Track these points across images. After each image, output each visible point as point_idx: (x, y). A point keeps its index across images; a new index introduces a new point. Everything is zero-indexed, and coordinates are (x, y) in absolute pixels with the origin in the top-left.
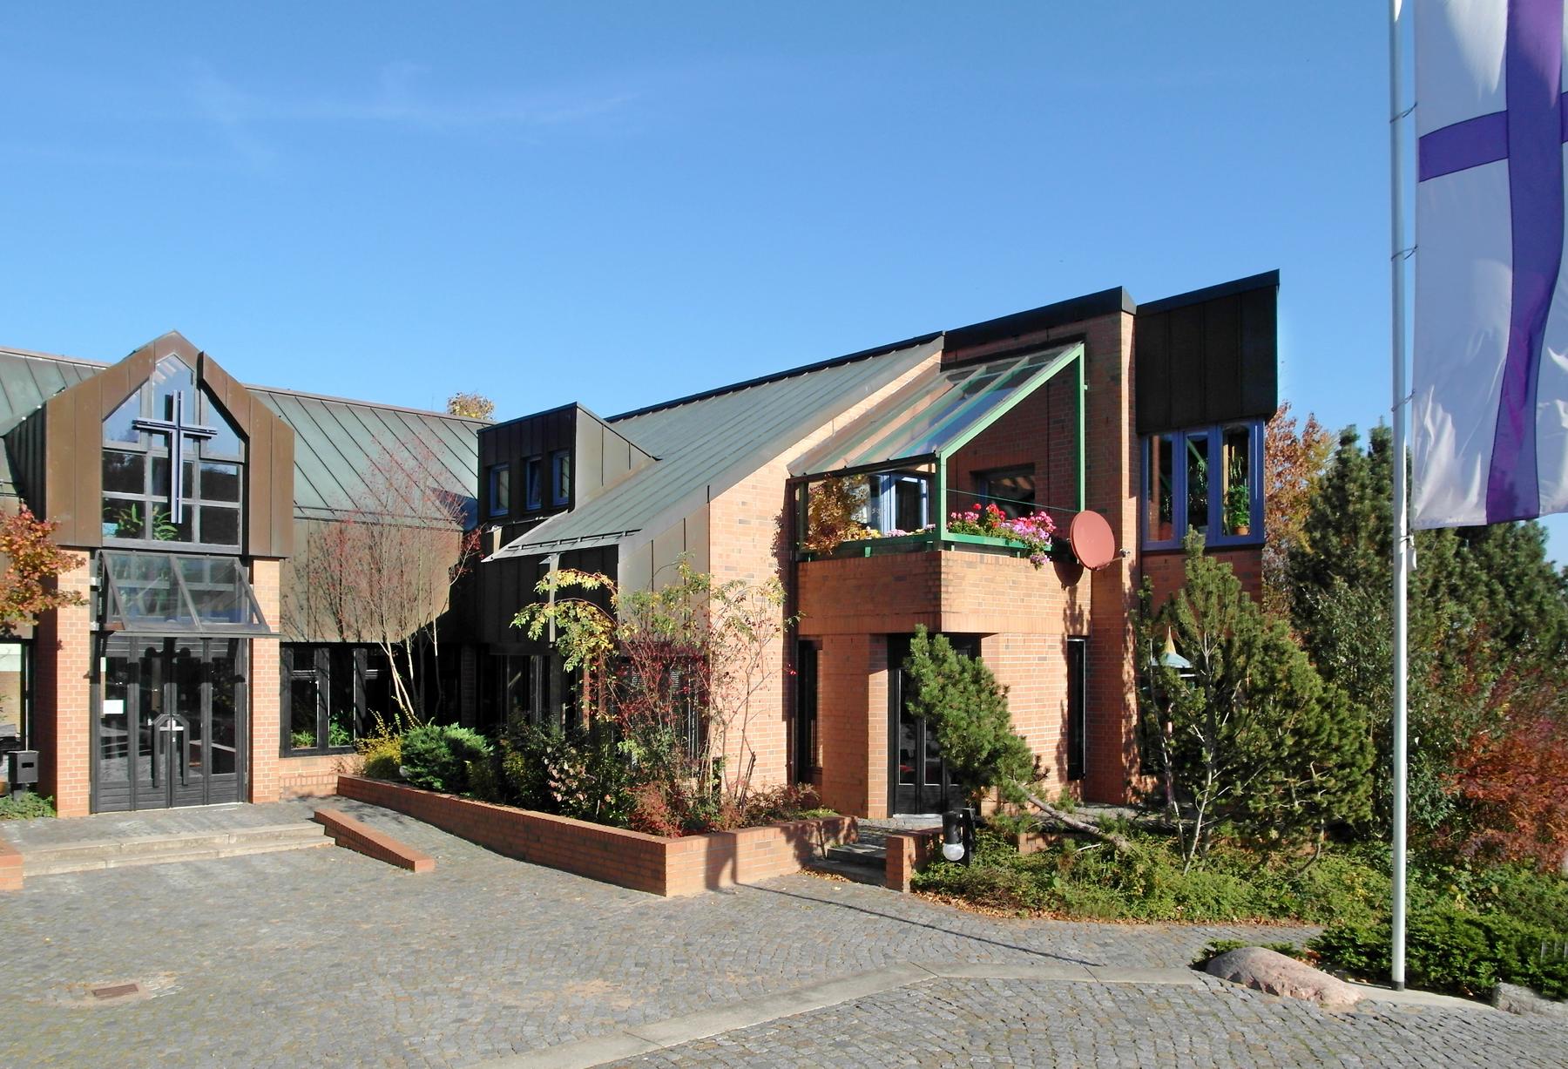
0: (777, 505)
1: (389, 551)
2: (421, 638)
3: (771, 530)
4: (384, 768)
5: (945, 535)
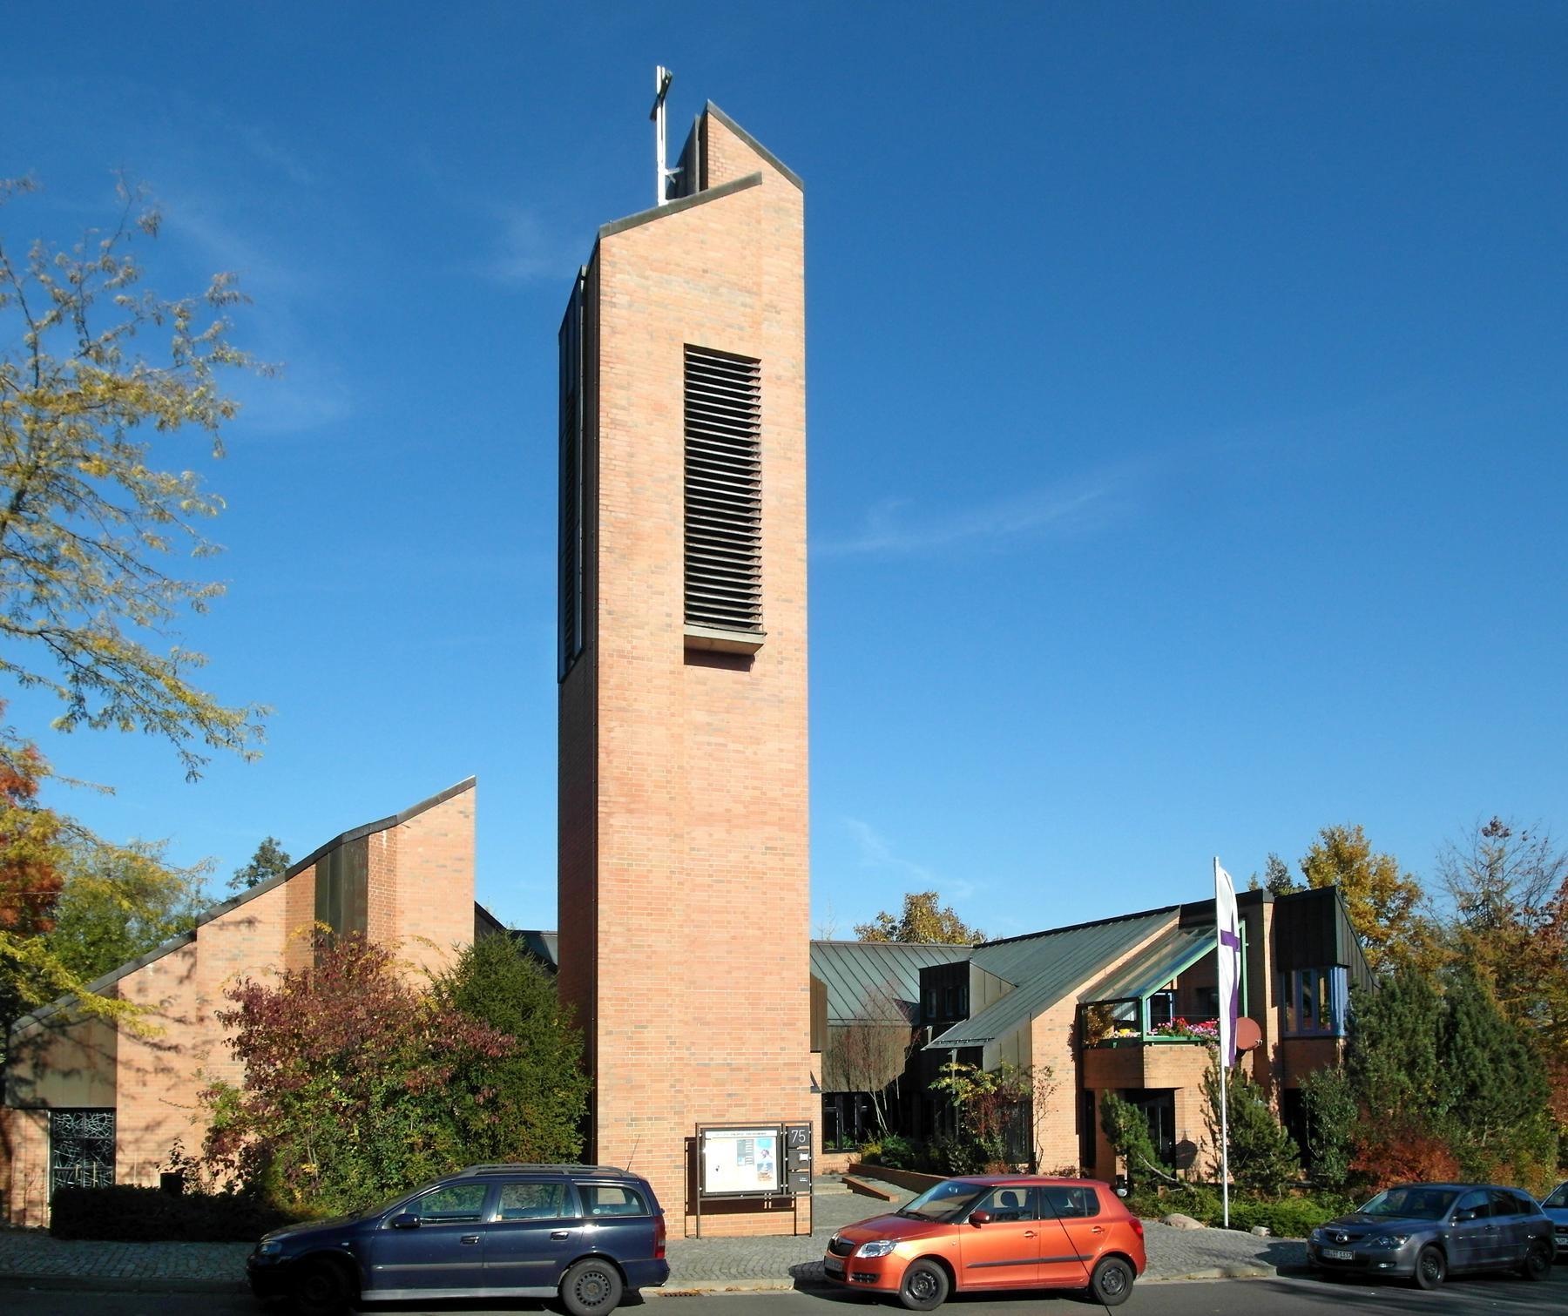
0: (1070, 1018)
1: (873, 1043)
2: (891, 1088)
3: (1068, 1032)
4: (873, 1159)
5: (1146, 1038)
